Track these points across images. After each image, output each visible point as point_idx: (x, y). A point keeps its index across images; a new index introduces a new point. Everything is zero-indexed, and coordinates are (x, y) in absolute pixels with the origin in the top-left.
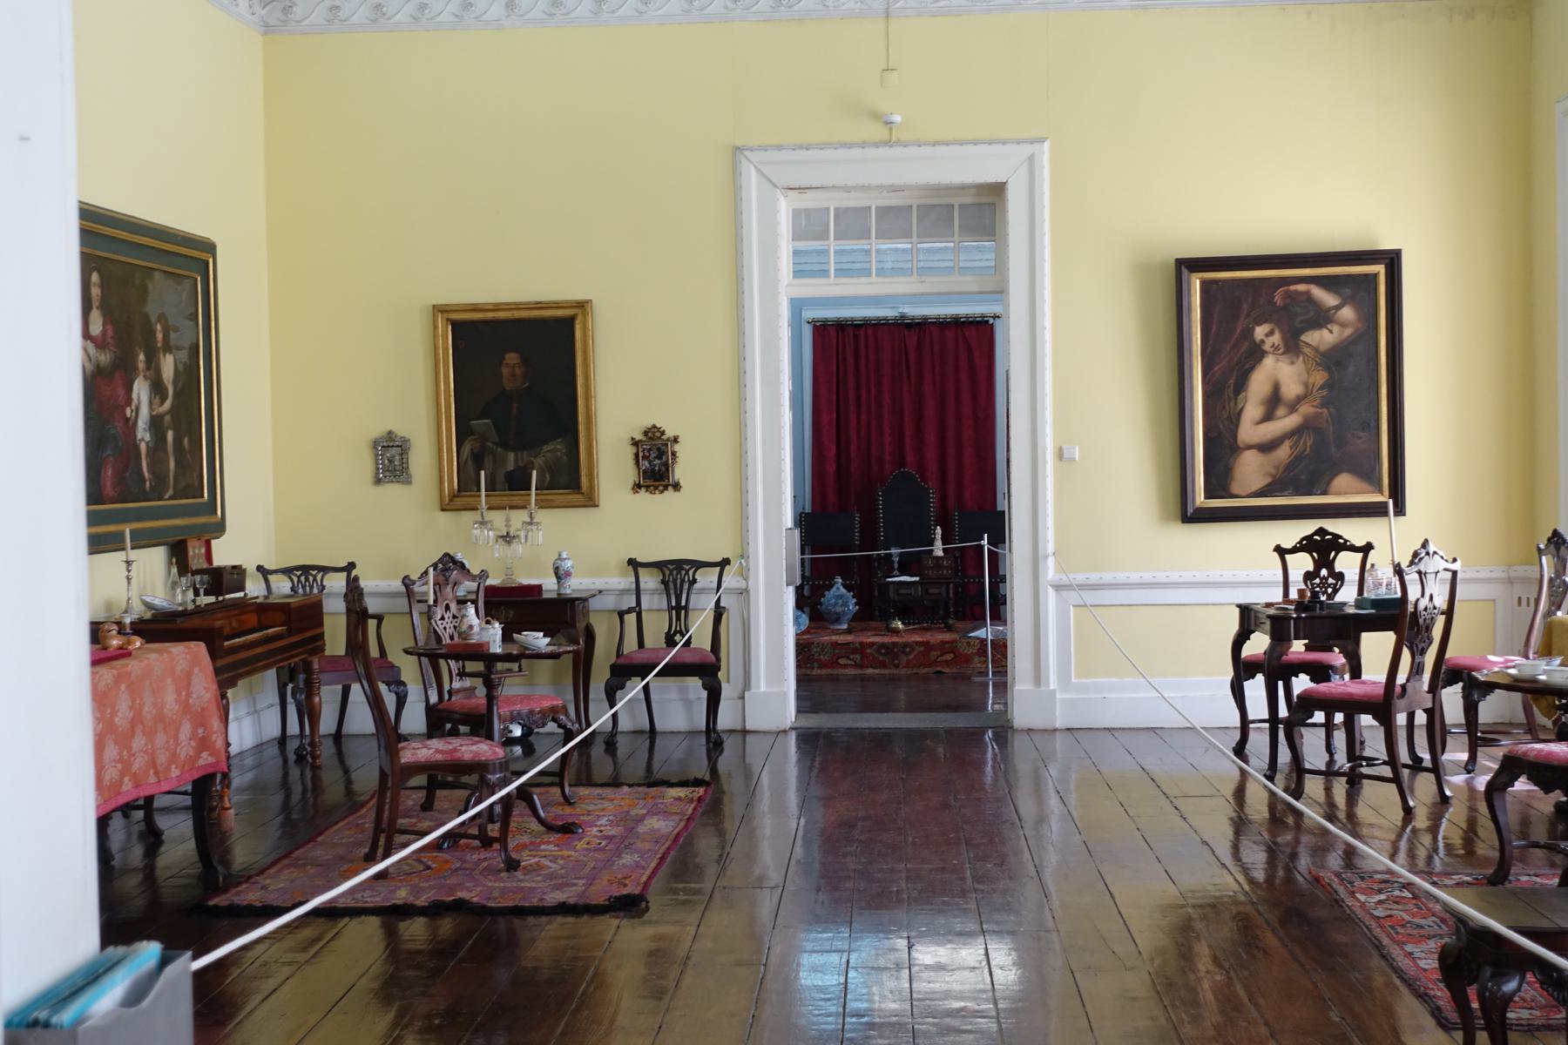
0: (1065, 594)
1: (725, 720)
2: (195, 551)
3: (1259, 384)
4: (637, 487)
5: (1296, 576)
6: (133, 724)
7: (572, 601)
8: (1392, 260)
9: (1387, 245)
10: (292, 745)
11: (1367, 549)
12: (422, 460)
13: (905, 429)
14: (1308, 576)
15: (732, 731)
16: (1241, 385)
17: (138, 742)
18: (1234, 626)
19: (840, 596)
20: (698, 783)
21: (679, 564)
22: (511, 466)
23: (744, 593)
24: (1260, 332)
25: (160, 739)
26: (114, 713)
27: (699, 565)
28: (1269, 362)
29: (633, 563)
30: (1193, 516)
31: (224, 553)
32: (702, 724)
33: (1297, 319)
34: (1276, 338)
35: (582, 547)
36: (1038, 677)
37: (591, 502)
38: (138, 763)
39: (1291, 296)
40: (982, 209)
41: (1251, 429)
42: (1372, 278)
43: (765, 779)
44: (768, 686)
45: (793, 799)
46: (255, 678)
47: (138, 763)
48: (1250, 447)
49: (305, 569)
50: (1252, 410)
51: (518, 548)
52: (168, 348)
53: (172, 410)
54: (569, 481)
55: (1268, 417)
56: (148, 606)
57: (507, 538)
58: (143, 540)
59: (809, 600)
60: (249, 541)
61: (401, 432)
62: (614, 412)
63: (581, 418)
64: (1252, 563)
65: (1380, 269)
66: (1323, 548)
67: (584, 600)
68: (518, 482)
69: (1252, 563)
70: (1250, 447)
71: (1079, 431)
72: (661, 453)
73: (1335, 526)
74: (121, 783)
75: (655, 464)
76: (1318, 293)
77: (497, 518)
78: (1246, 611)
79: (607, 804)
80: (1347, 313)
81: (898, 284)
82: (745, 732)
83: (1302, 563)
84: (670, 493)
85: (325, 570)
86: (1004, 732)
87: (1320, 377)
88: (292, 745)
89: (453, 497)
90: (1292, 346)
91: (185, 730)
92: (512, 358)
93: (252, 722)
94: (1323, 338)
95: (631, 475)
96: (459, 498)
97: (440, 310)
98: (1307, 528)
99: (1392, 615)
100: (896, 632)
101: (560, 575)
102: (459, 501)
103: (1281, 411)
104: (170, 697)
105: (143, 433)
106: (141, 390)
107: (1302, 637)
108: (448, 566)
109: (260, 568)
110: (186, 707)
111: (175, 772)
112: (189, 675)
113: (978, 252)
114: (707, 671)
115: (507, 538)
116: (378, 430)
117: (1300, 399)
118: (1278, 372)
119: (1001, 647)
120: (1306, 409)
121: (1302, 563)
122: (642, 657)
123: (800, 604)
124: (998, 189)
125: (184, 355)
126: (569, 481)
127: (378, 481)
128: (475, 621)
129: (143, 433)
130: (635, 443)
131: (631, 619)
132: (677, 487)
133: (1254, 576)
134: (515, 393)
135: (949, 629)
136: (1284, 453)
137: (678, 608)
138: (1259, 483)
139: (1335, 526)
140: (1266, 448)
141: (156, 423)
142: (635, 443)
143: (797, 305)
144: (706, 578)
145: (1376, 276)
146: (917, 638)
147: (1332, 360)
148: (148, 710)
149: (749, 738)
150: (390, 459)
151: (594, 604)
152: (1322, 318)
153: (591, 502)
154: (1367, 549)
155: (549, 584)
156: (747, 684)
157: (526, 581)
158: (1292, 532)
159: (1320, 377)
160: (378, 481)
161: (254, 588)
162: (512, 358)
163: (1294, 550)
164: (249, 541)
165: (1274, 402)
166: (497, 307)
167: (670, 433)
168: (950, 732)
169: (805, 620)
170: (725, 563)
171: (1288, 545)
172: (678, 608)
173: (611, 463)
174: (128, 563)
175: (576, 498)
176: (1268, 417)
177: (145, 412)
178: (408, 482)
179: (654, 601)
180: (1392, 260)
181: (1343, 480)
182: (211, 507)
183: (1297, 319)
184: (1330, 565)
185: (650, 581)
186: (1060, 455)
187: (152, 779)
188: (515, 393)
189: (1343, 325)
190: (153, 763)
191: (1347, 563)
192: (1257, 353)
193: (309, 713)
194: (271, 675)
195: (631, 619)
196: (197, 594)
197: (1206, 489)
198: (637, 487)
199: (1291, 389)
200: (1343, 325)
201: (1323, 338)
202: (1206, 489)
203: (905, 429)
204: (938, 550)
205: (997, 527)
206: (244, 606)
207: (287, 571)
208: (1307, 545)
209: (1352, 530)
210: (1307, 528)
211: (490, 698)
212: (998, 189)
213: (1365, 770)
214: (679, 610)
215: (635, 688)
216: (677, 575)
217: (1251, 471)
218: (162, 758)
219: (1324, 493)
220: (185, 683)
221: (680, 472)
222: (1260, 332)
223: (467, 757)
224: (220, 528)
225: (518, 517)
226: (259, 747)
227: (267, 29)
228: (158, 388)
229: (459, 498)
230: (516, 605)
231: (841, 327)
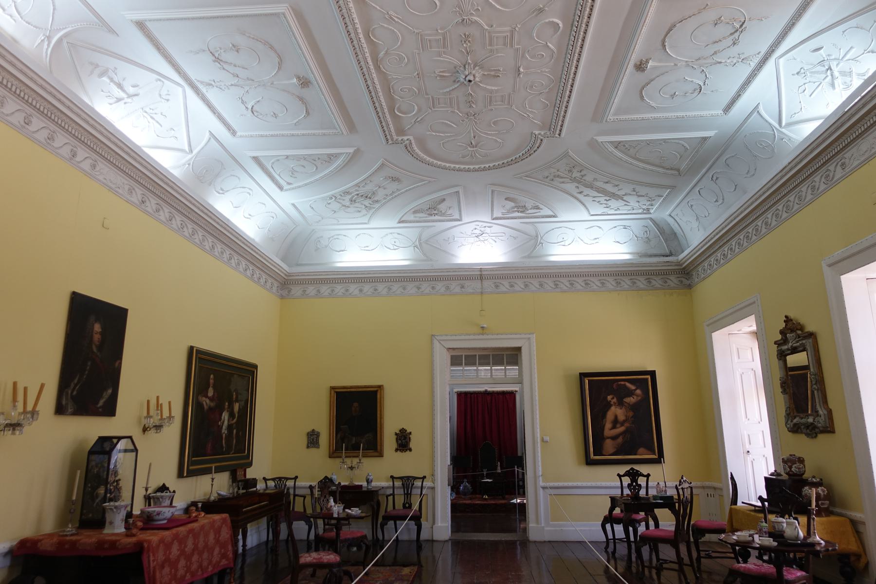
0: (546, 490)
1: (424, 535)
2: (240, 473)
3: (610, 416)
4: (397, 450)
5: (625, 484)
6: (193, 550)
7: (373, 491)
8: (653, 374)
9: (650, 368)
10: (270, 545)
11: (648, 476)
12: (324, 440)
13: (487, 432)
14: (629, 486)
15: (428, 541)
16: (604, 416)
17: (195, 558)
18: (609, 505)
19: (465, 485)
20: (414, 565)
21: (408, 478)
22: (354, 442)
23: (433, 488)
24: (609, 398)
25: (205, 555)
26: (186, 546)
27: (415, 478)
28: (613, 408)
29: (392, 477)
30: (589, 462)
31: (251, 473)
32: (415, 537)
33: (622, 394)
34: (615, 400)
35: (377, 472)
36: (537, 521)
37: (381, 455)
38: (194, 567)
39: (618, 385)
40: (512, 356)
41: (608, 431)
42: (645, 380)
43: (440, 563)
44: (440, 524)
45: (450, 567)
46: (260, 520)
47: (194, 567)
48: (608, 438)
49: (280, 479)
50: (608, 425)
51: (356, 471)
52: (237, 401)
53: (237, 423)
54: (374, 448)
55: (614, 427)
56: (219, 494)
57: (352, 468)
58: (219, 470)
59: (455, 488)
60: (262, 468)
61: (317, 430)
62: (390, 426)
63: (378, 425)
64: (609, 480)
65: (649, 377)
66: (634, 475)
67: (377, 491)
68: (356, 448)
69: (609, 480)
70: (608, 438)
71: (549, 432)
72: (405, 438)
73: (637, 467)
74: (185, 576)
75: (403, 441)
76: (628, 384)
77: (348, 461)
78: (613, 500)
79: (380, 575)
80: (638, 392)
81: (486, 379)
82: (433, 541)
83: (627, 481)
84: (408, 452)
85: (287, 479)
86: (525, 542)
87: (631, 414)
88: (270, 545)
89: (333, 453)
90: (620, 403)
91: (217, 551)
92: (356, 404)
93: (255, 535)
94: (631, 400)
95: (395, 446)
96: (334, 453)
97: (332, 388)
98: (627, 468)
99: (667, 502)
100: (485, 499)
101: (368, 481)
102: (335, 455)
103: (618, 425)
104: (212, 537)
105: (224, 430)
106: (225, 416)
107: (631, 507)
108: (326, 483)
109: (264, 478)
110: (217, 541)
111: (210, 569)
112: (220, 528)
113: (512, 371)
114: (417, 518)
115: (352, 468)
116: (309, 430)
117: (624, 421)
118: (616, 412)
119: (523, 507)
120: (627, 425)
121: (627, 481)
122: (395, 513)
123: (452, 490)
124: (519, 349)
125: (243, 403)
126: (374, 448)
127: (308, 447)
128: (333, 504)
129: (224, 430)
130: (396, 434)
131: (391, 498)
132: (410, 450)
133: (608, 484)
134: (356, 416)
135: (504, 498)
136: (620, 440)
137: (407, 494)
138: (612, 451)
139: (637, 467)
140: (614, 438)
141: (230, 427)
142: (396, 434)
143: (452, 386)
144: (418, 483)
145: (647, 379)
146: (493, 502)
147: (634, 407)
148: (201, 544)
149: (435, 544)
150: (313, 439)
151: (380, 492)
152: (631, 393)
153: (381, 455)
154: (648, 476)
155: (365, 484)
156: (434, 523)
157: (357, 484)
158: (623, 469)
159: (631, 414)
160: (308, 447)
161: (260, 486)
162: (356, 404)
163: (624, 476)
164: (262, 468)
165: (615, 422)
166: (351, 387)
167: (408, 431)
168: (506, 542)
169: (454, 495)
170: (424, 477)
171: (622, 474)
172: (407, 494)
173: (389, 442)
174: (213, 479)
175: (376, 454)
176: (614, 427)
177: (226, 423)
178: (318, 447)
179: (399, 492)
180: (653, 374)
181: (641, 450)
182: (248, 457)
183: (622, 394)
184: (636, 482)
185: (398, 484)
186: (543, 440)
187: (200, 573)
188: (356, 416)
189: (637, 396)
190: (200, 566)
191: (642, 481)
192: (608, 405)
193: (276, 534)
194: (266, 518)
195: (391, 498)
196: (239, 489)
197: (594, 454)
198: (397, 450)
199: (621, 418)
200: (637, 396)
201: (631, 400)
202: (594, 454)
203: (487, 432)
204: (499, 471)
205: (520, 461)
206: (256, 493)
207: (273, 479)
208: (627, 474)
209: (643, 469)
210: (627, 468)
211: (338, 534)
212: (519, 349)
213: (665, 566)
214: (408, 495)
215: (391, 523)
216: (408, 482)
217: (609, 445)
218: (205, 564)
219: (636, 454)
220: (218, 532)
221: (412, 445)
222: (609, 398)
223: (325, 561)
224: (250, 464)
225: (355, 461)
226: (258, 546)
227: (282, 297)
228: (232, 415)
229: (334, 453)
230: (352, 495)
231: (466, 394)
